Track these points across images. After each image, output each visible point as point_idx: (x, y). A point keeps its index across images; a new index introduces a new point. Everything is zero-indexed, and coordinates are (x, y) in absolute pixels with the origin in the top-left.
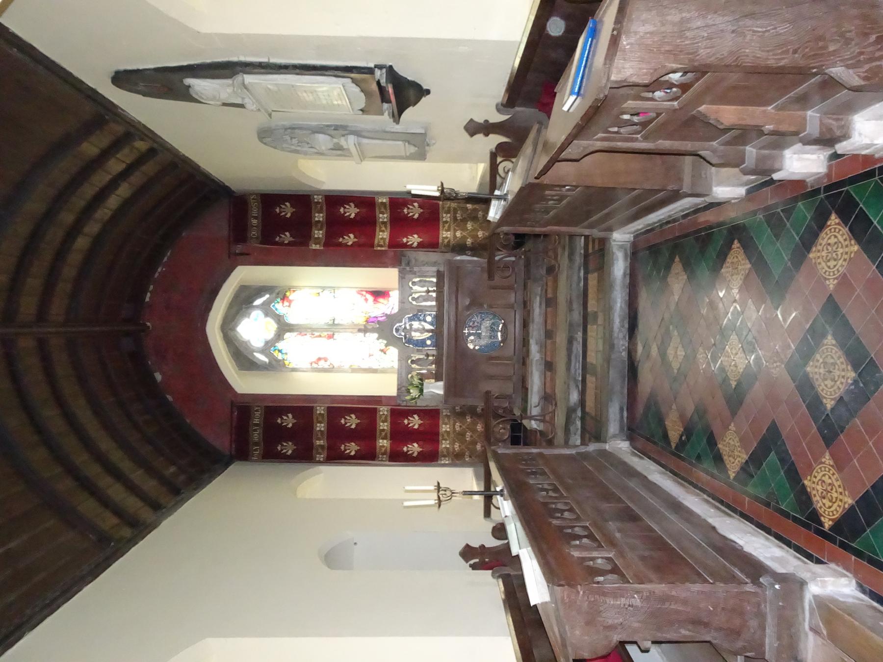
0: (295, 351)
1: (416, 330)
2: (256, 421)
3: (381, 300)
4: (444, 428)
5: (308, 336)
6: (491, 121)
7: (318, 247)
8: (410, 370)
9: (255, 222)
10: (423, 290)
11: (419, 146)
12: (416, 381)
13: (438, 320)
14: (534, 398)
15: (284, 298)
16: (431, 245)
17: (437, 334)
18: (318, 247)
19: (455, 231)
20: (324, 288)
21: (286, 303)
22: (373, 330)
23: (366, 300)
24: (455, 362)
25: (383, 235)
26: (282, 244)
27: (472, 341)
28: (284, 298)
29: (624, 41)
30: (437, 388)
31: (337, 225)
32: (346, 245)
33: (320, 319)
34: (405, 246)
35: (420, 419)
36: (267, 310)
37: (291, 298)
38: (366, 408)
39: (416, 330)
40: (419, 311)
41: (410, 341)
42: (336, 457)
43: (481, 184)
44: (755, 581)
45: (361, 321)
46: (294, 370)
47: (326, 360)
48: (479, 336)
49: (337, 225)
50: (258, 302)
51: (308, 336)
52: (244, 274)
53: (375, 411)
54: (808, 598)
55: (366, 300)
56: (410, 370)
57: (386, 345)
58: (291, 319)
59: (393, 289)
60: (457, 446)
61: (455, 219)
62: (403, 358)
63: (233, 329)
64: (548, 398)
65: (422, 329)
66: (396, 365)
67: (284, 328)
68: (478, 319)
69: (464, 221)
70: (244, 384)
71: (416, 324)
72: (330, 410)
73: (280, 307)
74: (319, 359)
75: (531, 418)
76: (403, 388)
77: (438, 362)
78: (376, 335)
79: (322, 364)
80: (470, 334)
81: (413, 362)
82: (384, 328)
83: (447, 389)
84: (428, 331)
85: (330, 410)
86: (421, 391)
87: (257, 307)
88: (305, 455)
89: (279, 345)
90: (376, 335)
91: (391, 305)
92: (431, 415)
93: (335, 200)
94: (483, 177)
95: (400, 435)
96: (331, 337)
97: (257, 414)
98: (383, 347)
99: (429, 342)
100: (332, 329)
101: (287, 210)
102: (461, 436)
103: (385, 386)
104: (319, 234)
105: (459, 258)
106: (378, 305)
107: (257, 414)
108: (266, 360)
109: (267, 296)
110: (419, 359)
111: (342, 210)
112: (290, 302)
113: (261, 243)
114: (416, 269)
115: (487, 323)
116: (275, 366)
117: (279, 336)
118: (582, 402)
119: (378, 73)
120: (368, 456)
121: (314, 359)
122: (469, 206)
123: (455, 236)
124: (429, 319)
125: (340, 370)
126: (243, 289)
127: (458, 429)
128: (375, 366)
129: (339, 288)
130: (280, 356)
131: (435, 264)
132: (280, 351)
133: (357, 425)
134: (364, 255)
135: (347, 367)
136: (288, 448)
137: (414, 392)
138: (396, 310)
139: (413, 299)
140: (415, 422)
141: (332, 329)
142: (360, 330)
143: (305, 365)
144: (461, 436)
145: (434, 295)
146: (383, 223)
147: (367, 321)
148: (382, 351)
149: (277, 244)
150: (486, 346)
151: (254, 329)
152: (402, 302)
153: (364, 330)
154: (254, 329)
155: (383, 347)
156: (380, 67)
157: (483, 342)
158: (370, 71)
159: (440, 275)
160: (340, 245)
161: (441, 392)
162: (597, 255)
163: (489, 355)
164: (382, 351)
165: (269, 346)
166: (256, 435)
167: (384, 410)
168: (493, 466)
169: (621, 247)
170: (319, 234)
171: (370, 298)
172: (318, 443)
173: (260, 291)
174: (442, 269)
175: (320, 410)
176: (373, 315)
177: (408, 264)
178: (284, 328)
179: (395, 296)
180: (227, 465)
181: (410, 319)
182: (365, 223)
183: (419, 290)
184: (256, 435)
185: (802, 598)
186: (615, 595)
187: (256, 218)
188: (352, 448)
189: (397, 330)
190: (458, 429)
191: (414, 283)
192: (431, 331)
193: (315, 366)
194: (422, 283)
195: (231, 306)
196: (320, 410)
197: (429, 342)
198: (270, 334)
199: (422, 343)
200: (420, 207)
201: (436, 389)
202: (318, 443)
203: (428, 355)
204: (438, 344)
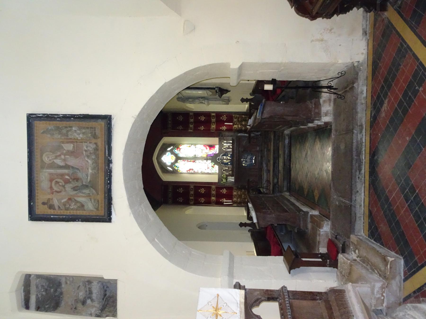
0: (183, 167)
1: (225, 159)
2: (170, 190)
3: (212, 149)
4: (235, 193)
5: (186, 162)
6: (249, 98)
7: (191, 131)
8: (223, 173)
9: (170, 122)
10: (227, 145)
11: (228, 101)
12: (225, 177)
13: (232, 156)
14: (264, 181)
15: (178, 148)
16: (230, 129)
17: (232, 161)
18: (191, 131)
19: (238, 125)
20: (192, 144)
21: (179, 150)
22: (210, 159)
23: (207, 148)
24: (237, 168)
25: (213, 126)
26: (179, 130)
27: (244, 163)
28: (178, 148)
29: (264, 112)
30: (231, 179)
31: (198, 123)
32: (201, 130)
33: (191, 155)
34: (221, 130)
35: (226, 190)
36: (172, 152)
37: (180, 148)
38: (207, 186)
39: (225, 159)
40: (226, 153)
41: (223, 163)
42: (197, 203)
43: (247, 110)
44: (299, 213)
45: (205, 156)
46: (181, 173)
47: (192, 170)
48: (246, 161)
49: (198, 123)
50: (169, 149)
51: (186, 162)
52: (166, 140)
53: (210, 187)
54: (309, 215)
55: (207, 148)
56: (223, 173)
57: (214, 165)
58: (181, 155)
59: (216, 145)
60: (239, 200)
61: (238, 121)
62: (220, 169)
63: (160, 159)
64: (268, 181)
65: (227, 159)
66: (217, 172)
67: (178, 158)
68: (246, 156)
69: (242, 121)
70: (166, 178)
71: (225, 157)
72: (195, 186)
73: (176, 151)
74: (190, 169)
75: (263, 188)
76: (220, 179)
77: (232, 170)
78: (210, 161)
79: (191, 171)
80: (243, 161)
81: (224, 170)
82: (214, 158)
83: (235, 179)
84: (229, 160)
85: (195, 186)
86: (227, 180)
87: (169, 151)
88: (187, 203)
89: (176, 164)
90: (210, 161)
91: (216, 150)
92: (230, 189)
93: (197, 114)
94: (247, 108)
95: (219, 196)
96: (194, 162)
97: (170, 188)
98: (213, 165)
99: (229, 164)
100: (194, 159)
101: (181, 118)
102: (240, 196)
103: (215, 179)
104: (191, 126)
105: (239, 134)
106: (212, 151)
107: (170, 188)
108: (172, 170)
109: (172, 147)
110: (226, 170)
111: (199, 118)
112: (180, 149)
113: (172, 129)
114: (225, 138)
115: (249, 157)
116: (175, 172)
117: (176, 161)
118: (278, 182)
119: (216, 89)
120: (208, 203)
121: (188, 169)
122: (243, 116)
123: (238, 127)
124: (229, 155)
125: (197, 173)
126: (164, 144)
127: (239, 194)
128: (210, 172)
129: (197, 144)
130: (176, 169)
131: (231, 136)
132: (176, 166)
133: (204, 192)
134: (207, 134)
135: (200, 172)
136: (181, 200)
137: (224, 180)
138: (217, 152)
139: (224, 148)
140: (224, 191)
141: (194, 159)
142: (205, 159)
143: (185, 171)
144: (240, 196)
145: (231, 147)
146: (214, 122)
147: (207, 156)
148: (212, 166)
149: (177, 129)
150: (249, 165)
151: (168, 159)
152: (220, 149)
153: (207, 159)
154: (168, 159)
155: (213, 165)
156: (217, 87)
157: (248, 163)
158: (214, 89)
159: (233, 140)
160: (199, 130)
161: (233, 180)
162: (279, 137)
163: (250, 167)
164: (212, 166)
165: (173, 164)
166: (170, 195)
167: (213, 187)
168: (250, 205)
169: (287, 135)
170: (191, 126)
171: (208, 148)
172: (191, 198)
173: (170, 145)
174: (234, 138)
175: (192, 187)
176: (209, 154)
177: (222, 136)
178: (178, 158)
179: (217, 147)
180: (160, 206)
181: (223, 155)
182: (207, 123)
183: (226, 145)
184: (170, 195)
185: (308, 215)
186: (269, 214)
187: (170, 121)
188: (203, 200)
189: (218, 159)
190: (239, 194)
191: (224, 143)
192: (230, 160)
193: (189, 172)
194: (227, 143)
195: (160, 150)
196: (192, 187)
197: (229, 164)
198: (173, 161)
199: (227, 164)
200: (226, 116)
201: (232, 179)
202: (191, 198)
203: (229, 168)
204: (232, 163)
